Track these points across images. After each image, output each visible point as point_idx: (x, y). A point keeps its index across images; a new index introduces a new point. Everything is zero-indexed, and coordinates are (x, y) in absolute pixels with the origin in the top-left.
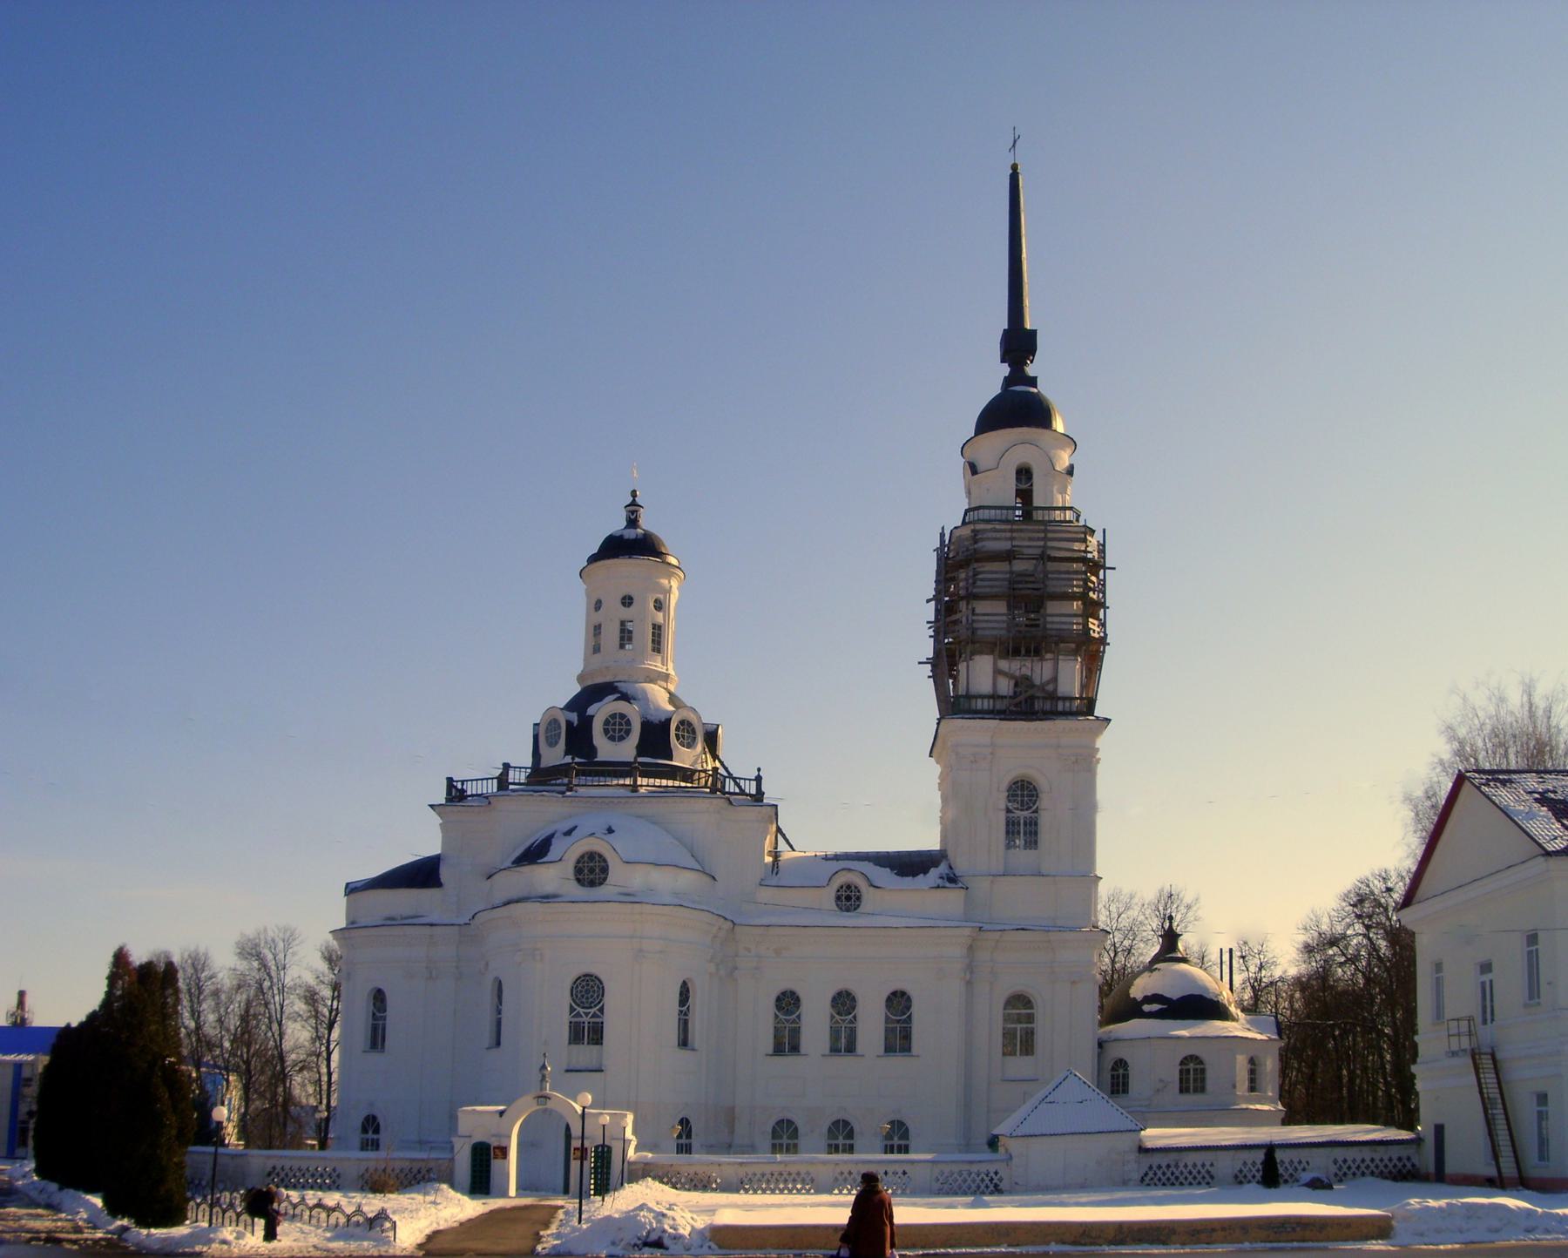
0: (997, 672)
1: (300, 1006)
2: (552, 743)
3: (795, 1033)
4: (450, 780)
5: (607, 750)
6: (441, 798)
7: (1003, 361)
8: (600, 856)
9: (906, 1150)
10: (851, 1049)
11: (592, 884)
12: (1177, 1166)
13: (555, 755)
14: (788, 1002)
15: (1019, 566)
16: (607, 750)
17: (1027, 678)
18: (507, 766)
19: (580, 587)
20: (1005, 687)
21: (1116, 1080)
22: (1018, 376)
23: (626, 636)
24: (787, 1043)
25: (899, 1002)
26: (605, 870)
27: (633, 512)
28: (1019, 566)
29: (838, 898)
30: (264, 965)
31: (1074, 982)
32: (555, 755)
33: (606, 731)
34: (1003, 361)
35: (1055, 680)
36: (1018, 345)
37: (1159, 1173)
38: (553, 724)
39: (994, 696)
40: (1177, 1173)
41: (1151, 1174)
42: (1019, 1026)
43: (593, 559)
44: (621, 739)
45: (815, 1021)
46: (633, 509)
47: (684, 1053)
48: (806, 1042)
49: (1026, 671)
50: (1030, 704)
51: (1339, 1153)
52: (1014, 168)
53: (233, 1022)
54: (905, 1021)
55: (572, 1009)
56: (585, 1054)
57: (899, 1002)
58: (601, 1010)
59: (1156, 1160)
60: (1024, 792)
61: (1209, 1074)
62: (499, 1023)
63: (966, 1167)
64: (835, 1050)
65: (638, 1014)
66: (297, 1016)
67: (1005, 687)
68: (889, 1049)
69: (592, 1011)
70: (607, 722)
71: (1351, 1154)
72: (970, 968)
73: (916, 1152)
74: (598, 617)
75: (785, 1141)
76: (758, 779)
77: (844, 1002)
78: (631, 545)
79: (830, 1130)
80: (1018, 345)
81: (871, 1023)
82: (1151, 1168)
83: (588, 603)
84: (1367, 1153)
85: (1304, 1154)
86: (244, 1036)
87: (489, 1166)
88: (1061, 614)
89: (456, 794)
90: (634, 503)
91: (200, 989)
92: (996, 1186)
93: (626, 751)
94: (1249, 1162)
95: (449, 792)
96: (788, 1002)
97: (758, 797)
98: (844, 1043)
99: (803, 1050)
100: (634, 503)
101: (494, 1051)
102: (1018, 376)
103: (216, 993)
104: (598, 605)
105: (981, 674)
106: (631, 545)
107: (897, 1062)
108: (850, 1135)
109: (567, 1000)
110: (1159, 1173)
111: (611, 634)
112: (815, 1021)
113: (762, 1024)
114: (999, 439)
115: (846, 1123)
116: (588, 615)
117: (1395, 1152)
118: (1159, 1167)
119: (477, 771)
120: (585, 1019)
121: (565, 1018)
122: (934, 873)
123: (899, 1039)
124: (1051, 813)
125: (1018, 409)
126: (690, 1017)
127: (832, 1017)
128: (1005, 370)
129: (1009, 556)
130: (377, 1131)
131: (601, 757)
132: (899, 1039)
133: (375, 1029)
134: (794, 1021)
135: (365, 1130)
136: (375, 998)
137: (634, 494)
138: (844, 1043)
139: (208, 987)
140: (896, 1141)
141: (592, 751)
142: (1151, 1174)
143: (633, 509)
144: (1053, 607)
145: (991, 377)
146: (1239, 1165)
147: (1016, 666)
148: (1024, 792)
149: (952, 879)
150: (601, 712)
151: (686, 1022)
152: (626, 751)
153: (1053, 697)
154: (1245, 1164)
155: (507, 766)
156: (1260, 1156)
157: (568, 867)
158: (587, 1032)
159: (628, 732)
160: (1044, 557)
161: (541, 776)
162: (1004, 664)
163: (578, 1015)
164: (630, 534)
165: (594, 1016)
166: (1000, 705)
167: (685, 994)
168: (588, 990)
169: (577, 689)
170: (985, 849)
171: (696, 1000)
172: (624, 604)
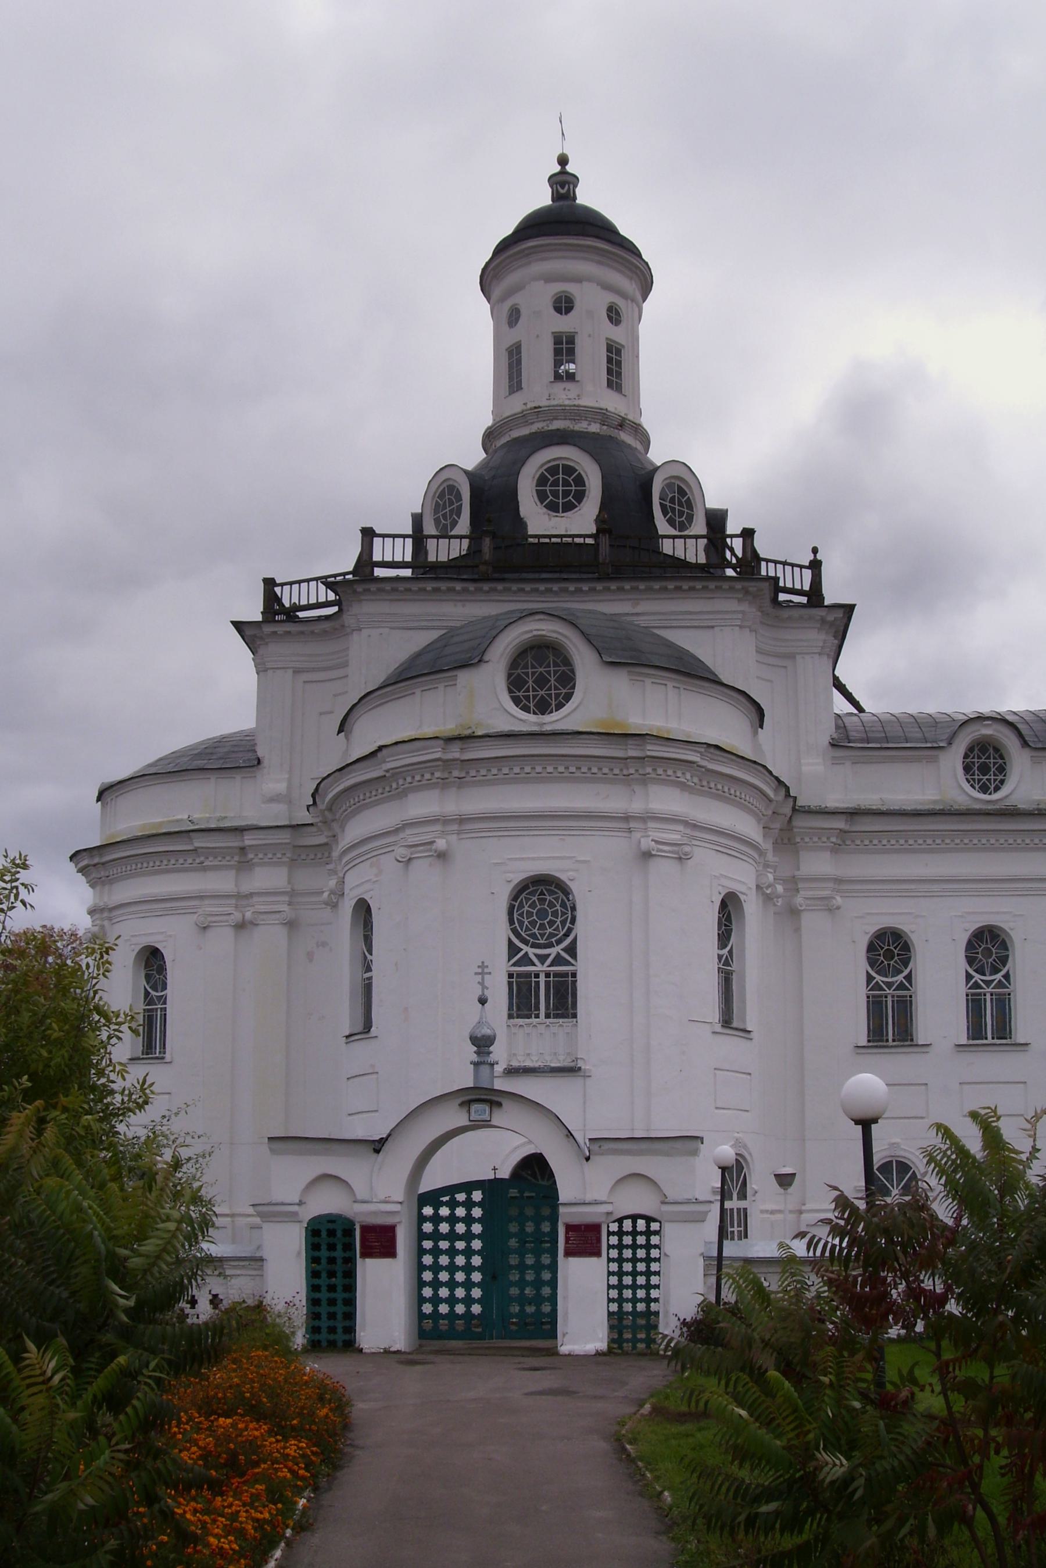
3: (905, 1008)
4: (270, 584)
14: (890, 950)
16: (539, 521)
18: (368, 534)
23: (564, 347)
24: (890, 1022)
25: (988, 948)
29: (967, 769)
33: (541, 496)
46: (563, 183)
47: (730, 1045)
55: (513, 950)
57: (988, 948)
58: (572, 950)
62: (724, 938)
64: (976, 1030)
69: (553, 951)
76: (815, 566)
78: (565, 225)
87: (350, 1274)
93: (581, 522)
96: (890, 950)
97: (815, 595)
101: (361, 1049)
106: (565, 225)
111: (539, 360)
120: (539, 967)
126: (734, 966)
127: (870, 978)
132: (990, 1020)
137: (563, 161)
143: (563, 183)
159: (580, 496)
163: (526, 960)
165: (558, 960)
172: (558, 310)
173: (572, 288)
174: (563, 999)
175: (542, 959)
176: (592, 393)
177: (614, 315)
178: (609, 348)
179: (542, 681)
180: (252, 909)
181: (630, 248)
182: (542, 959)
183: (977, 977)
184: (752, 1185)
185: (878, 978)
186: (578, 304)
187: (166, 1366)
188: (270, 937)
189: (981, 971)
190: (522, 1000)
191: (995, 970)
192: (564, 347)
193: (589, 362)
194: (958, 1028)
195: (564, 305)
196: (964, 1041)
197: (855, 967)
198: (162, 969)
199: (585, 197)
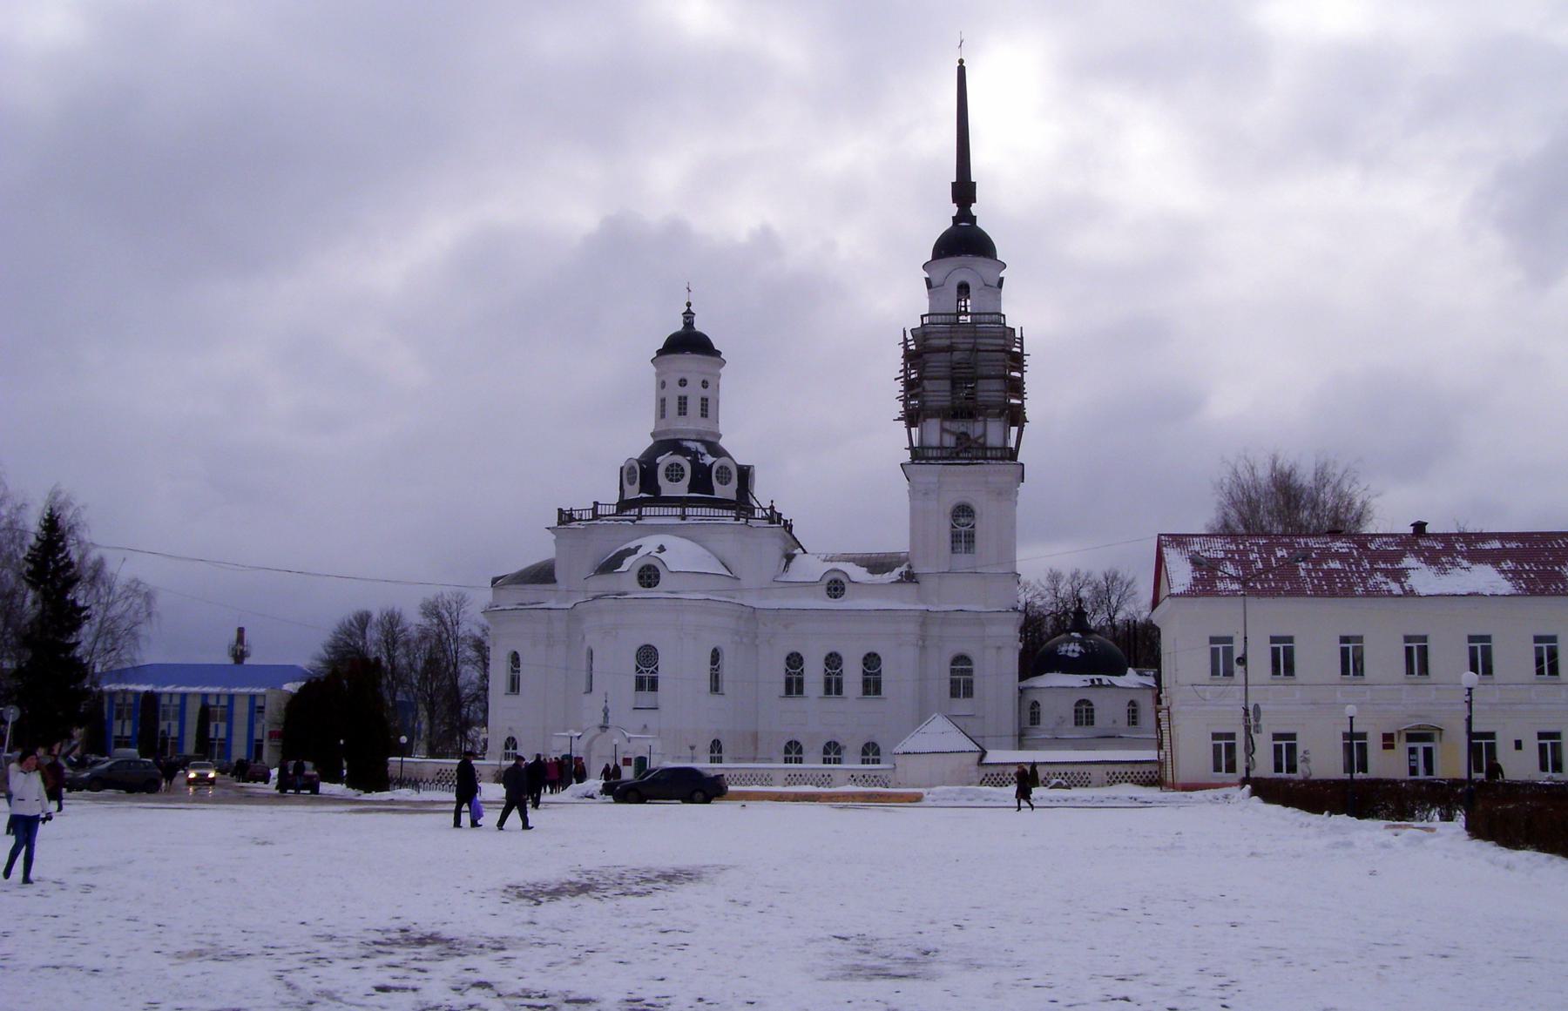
0: (943, 430)
1: (470, 653)
2: (632, 483)
5: (668, 488)
10: (839, 691)
11: (649, 586)
13: (633, 492)
14: (795, 661)
15: (957, 356)
17: (965, 434)
18: (596, 504)
20: (949, 441)
21: (1031, 714)
22: (964, 216)
23: (683, 403)
24: (794, 686)
25: (871, 661)
26: (658, 577)
28: (957, 356)
30: (442, 622)
31: (999, 648)
32: (633, 492)
35: (984, 435)
36: (964, 191)
38: (632, 468)
39: (941, 448)
43: (660, 353)
45: (814, 674)
46: (689, 316)
47: (716, 698)
49: (962, 429)
50: (968, 451)
51: (1110, 768)
52: (961, 61)
53: (420, 664)
56: (646, 697)
57: (871, 661)
59: (991, 770)
60: (963, 512)
61: (1096, 713)
65: (682, 668)
66: (468, 661)
67: (949, 441)
68: (866, 692)
71: (1118, 768)
72: (923, 638)
74: (664, 393)
77: (833, 661)
78: (689, 342)
80: (964, 191)
81: (852, 674)
84: (1128, 768)
85: (1086, 768)
86: (433, 664)
88: (989, 391)
89: (565, 517)
90: (689, 311)
91: (395, 642)
93: (680, 489)
95: (560, 517)
96: (795, 661)
98: (833, 686)
100: (689, 311)
102: (964, 216)
103: (407, 643)
104: (663, 385)
105: (933, 431)
106: (689, 342)
107: (872, 703)
109: (634, 663)
111: (672, 406)
112: (814, 674)
113: (777, 674)
117: (1147, 768)
119: (580, 502)
121: (633, 673)
122: (895, 575)
123: (872, 686)
124: (983, 527)
125: (965, 242)
129: (950, 349)
131: (663, 494)
132: (872, 686)
133: (513, 680)
135: (507, 747)
137: (689, 305)
138: (833, 686)
139: (402, 638)
140: (832, 756)
141: (658, 489)
143: (689, 316)
144: (983, 385)
145: (944, 215)
147: (958, 426)
148: (963, 512)
149: (910, 577)
150: (664, 461)
152: (680, 489)
153: (984, 447)
155: (596, 504)
157: (634, 576)
158: (645, 683)
160: (975, 350)
161: (624, 505)
162: (947, 425)
166: (945, 454)
167: (716, 656)
168: (647, 655)
169: (651, 442)
170: (936, 558)
171: (726, 662)
173: (687, 377)
174: (654, 686)
176: (688, 426)
177: (705, 384)
180: (452, 966)
181: (718, 353)
190: (640, 685)
192: (683, 403)
193: (694, 407)
194: (821, 688)
195: (683, 383)
196: (822, 693)
197: (782, 665)
199: (699, 326)
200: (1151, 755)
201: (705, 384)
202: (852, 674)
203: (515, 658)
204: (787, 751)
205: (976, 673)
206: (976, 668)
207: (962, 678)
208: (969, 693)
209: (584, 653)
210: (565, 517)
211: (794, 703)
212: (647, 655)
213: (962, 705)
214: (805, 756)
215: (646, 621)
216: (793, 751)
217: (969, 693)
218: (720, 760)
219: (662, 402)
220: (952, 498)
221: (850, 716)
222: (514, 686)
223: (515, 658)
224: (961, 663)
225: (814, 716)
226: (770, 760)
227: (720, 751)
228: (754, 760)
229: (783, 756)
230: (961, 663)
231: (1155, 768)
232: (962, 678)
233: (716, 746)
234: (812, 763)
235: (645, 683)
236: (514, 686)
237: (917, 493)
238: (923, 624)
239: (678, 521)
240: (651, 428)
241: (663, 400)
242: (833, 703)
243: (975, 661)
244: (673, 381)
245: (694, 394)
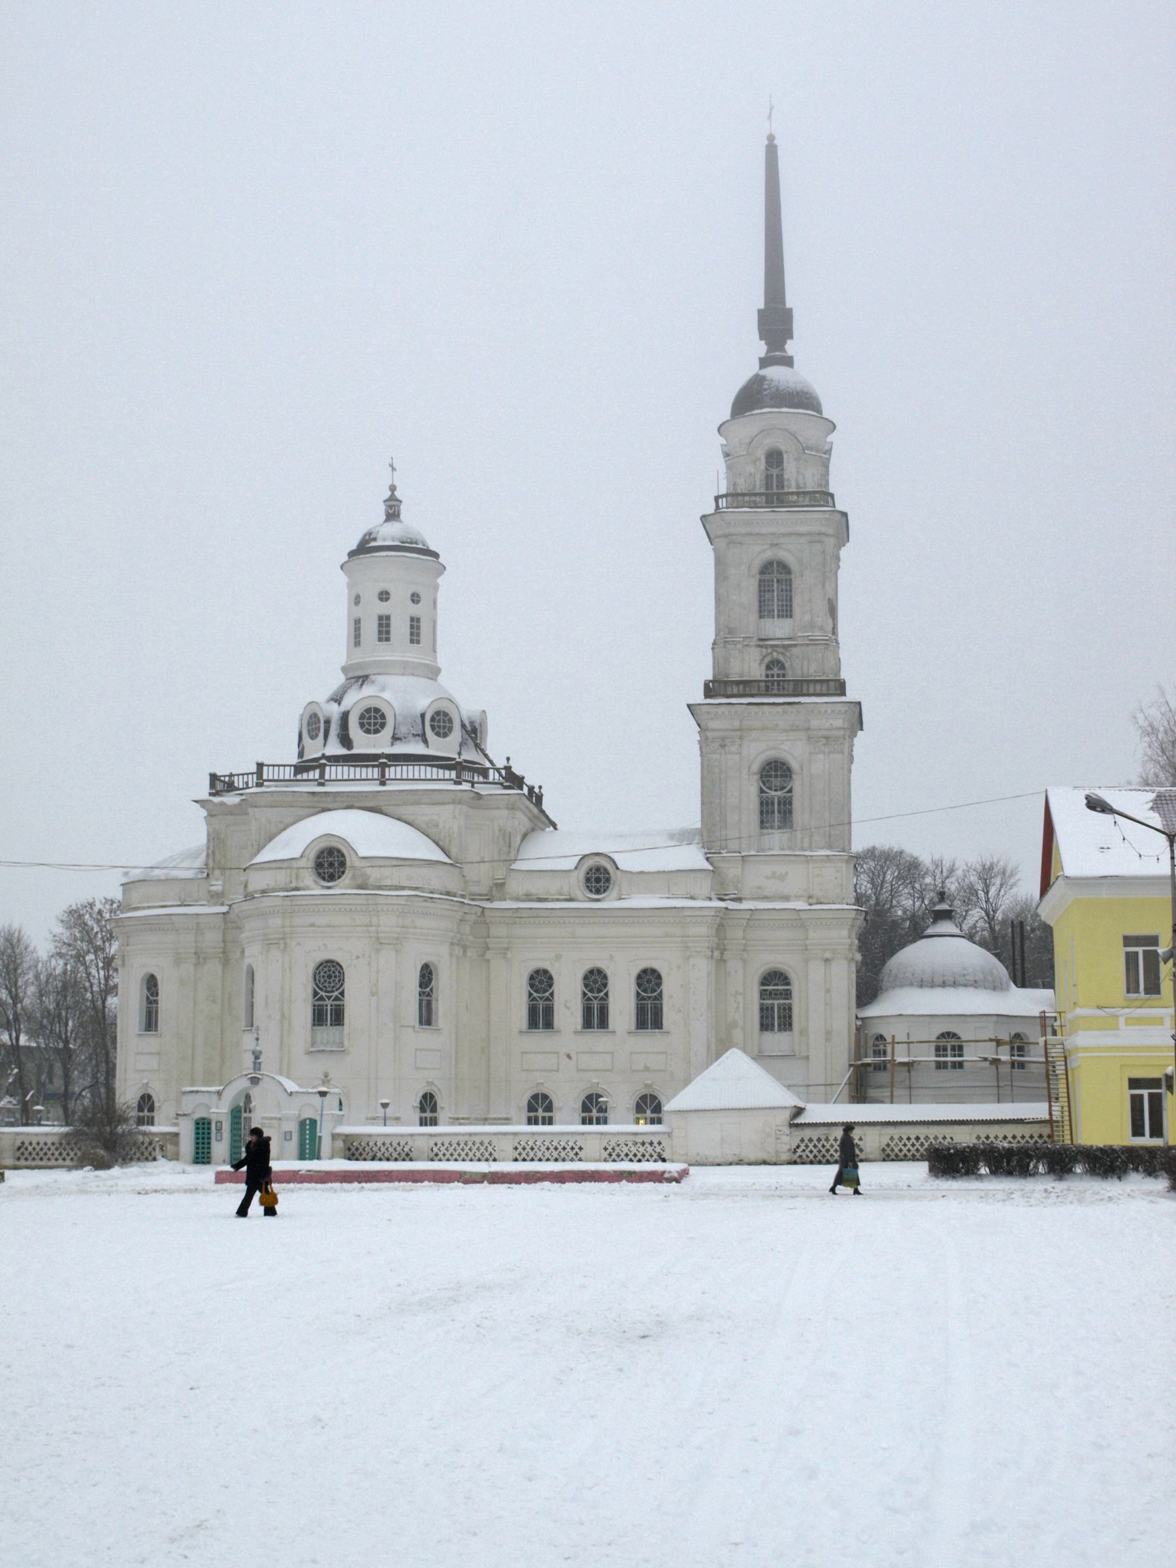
3: (549, 1011)
6: (204, 792)
7: (791, 310)
8: (339, 851)
9: (550, 1121)
10: (603, 1023)
12: (827, 1140)
14: (541, 981)
18: (260, 766)
19: (342, 579)
23: (384, 624)
24: (540, 1016)
25: (649, 981)
27: (391, 507)
29: (588, 880)
33: (362, 725)
34: (791, 310)
36: (775, 324)
37: (811, 1146)
40: (828, 1146)
41: (803, 1147)
42: (776, 1002)
43: (352, 554)
44: (377, 731)
47: (425, 1037)
48: (559, 1018)
52: (771, 138)
54: (655, 998)
55: (315, 994)
56: (328, 1033)
57: (649, 981)
58: (342, 994)
59: (808, 1133)
60: (776, 772)
63: (632, 1138)
65: (377, 990)
68: (588, 1024)
70: (362, 717)
73: (617, 1123)
74: (358, 612)
75: (541, 1113)
77: (595, 981)
79: (529, 1103)
80: (775, 324)
81: (622, 1001)
82: (802, 1140)
83: (349, 596)
89: (220, 784)
92: (407, 1155)
94: (896, 1137)
95: (212, 786)
96: (541, 981)
98: (595, 1016)
99: (556, 1024)
104: (357, 600)
107: (649, 1041)
108: (549, 1108)
110: (811, 1146)
111: (370, 629)
114: (750, 426)
115: (545, 1097)
116: (349, 609)
118: (811, 1140)
119: (239, 764)
123: (649, 1015)
128: (761, 349)
130: (151, 1109)
132: (649, 1015)
134: (547, 999)
135: (423, 1109)
136: (148, 982)
137: (393, 488)
138: (595, 1016)
140: (428, 1115)
142: (803, 1147)
145: (744, 356)
146: (886, 1140)
148: (776, 772)
151: (429, 1003)
154: (892, 1139)
155: (260, 766)
156: (839, 1133)
158: (328, 1011)
164: (389, 533)
165: (337, 999)
167: (427, 975)
168: (329, 976)
171: (443, 983)
172: (387, 593)
175: (329, 998)
178: (412, 619)
179: (331, 865)
182: (329, 998)
183: (590, 994)
184: (440, 1103)
185: (535, 994)
186: (392, 596)
187: (872, 902)
188: (214, 968)
189: (591, 991)
190: (319, 1018)
191: (599, 991)
192: (384, 624)
193: (400, 629)
195: (384, 596)
196: (579, 1027)
198: (156, 985)
200: (1037, 1110)
201: (415, 598)
202: (622, 1001)
203: (152, 983)
204: (531, 1108)
205: (795, 994)
206: (795, 988)
207: (776, 1005)
208: (786, 1023)
209: (244, 975)
210: (220, 784)
211: (540, 1040)
212: (329, 976)
213: (777, 1041)
214: (557, 1115)
215: (330, 928)
216: (540, 1107)
217: (786, 1023)
218: (434, 1122)
219: (357, 625)
220: (757, 751)
221: (618, 1056)
222: (150, 1022)
223: (152, 983)
224: (775, 983)
225: (569, 1058)
226: (507, 1120)
227: (434, 1110)
228: (485, 1121)
229: (524, 1115)
230: (775, 983)
231: (1046, 1131)
232: (776, 1005)
233: (428, 1105)
234: (566, 1126)
235: (328, 1011)
236: (150, 1022)
237: (711, 743)
238: (721, 928)
239: (375, 787)
240: (342, 660)
241: (357, 622)
242: (597, 1040)
243: (792, 976)
244: (370, 595)
245: (400, 612)
